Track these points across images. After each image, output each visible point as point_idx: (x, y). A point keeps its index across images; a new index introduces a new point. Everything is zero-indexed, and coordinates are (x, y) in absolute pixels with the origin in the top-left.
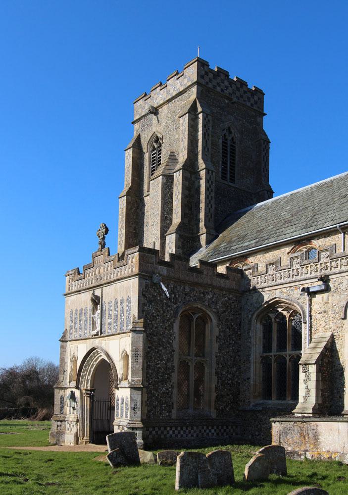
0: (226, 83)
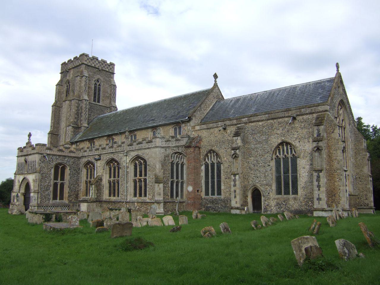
0: (97, 62)
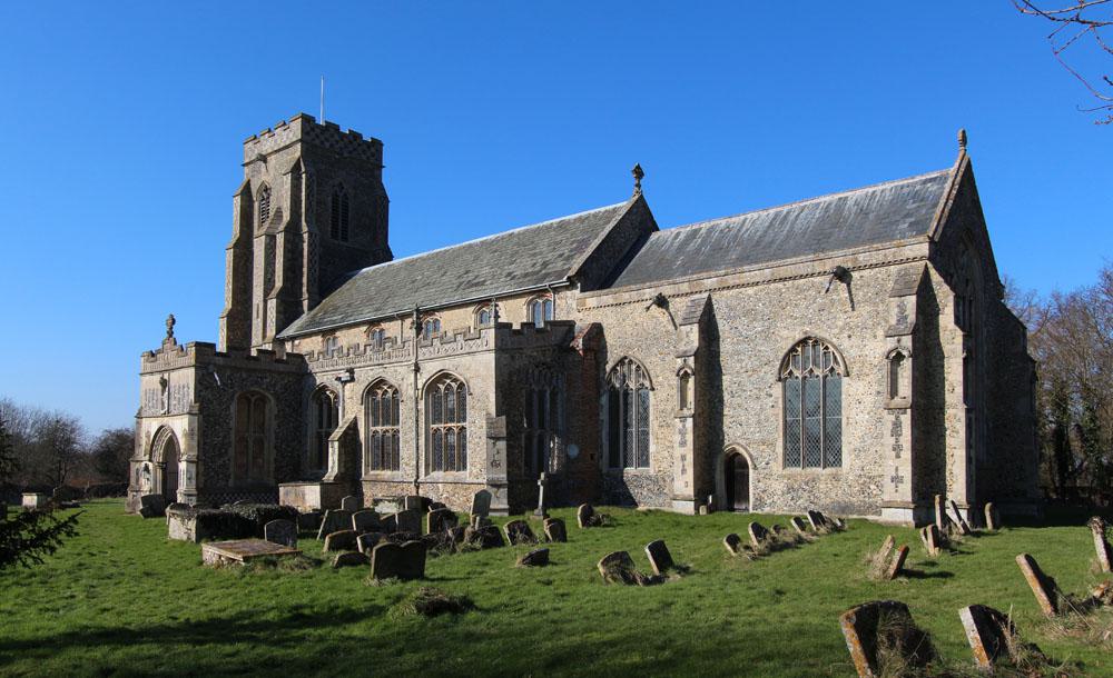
0: (337, 137)
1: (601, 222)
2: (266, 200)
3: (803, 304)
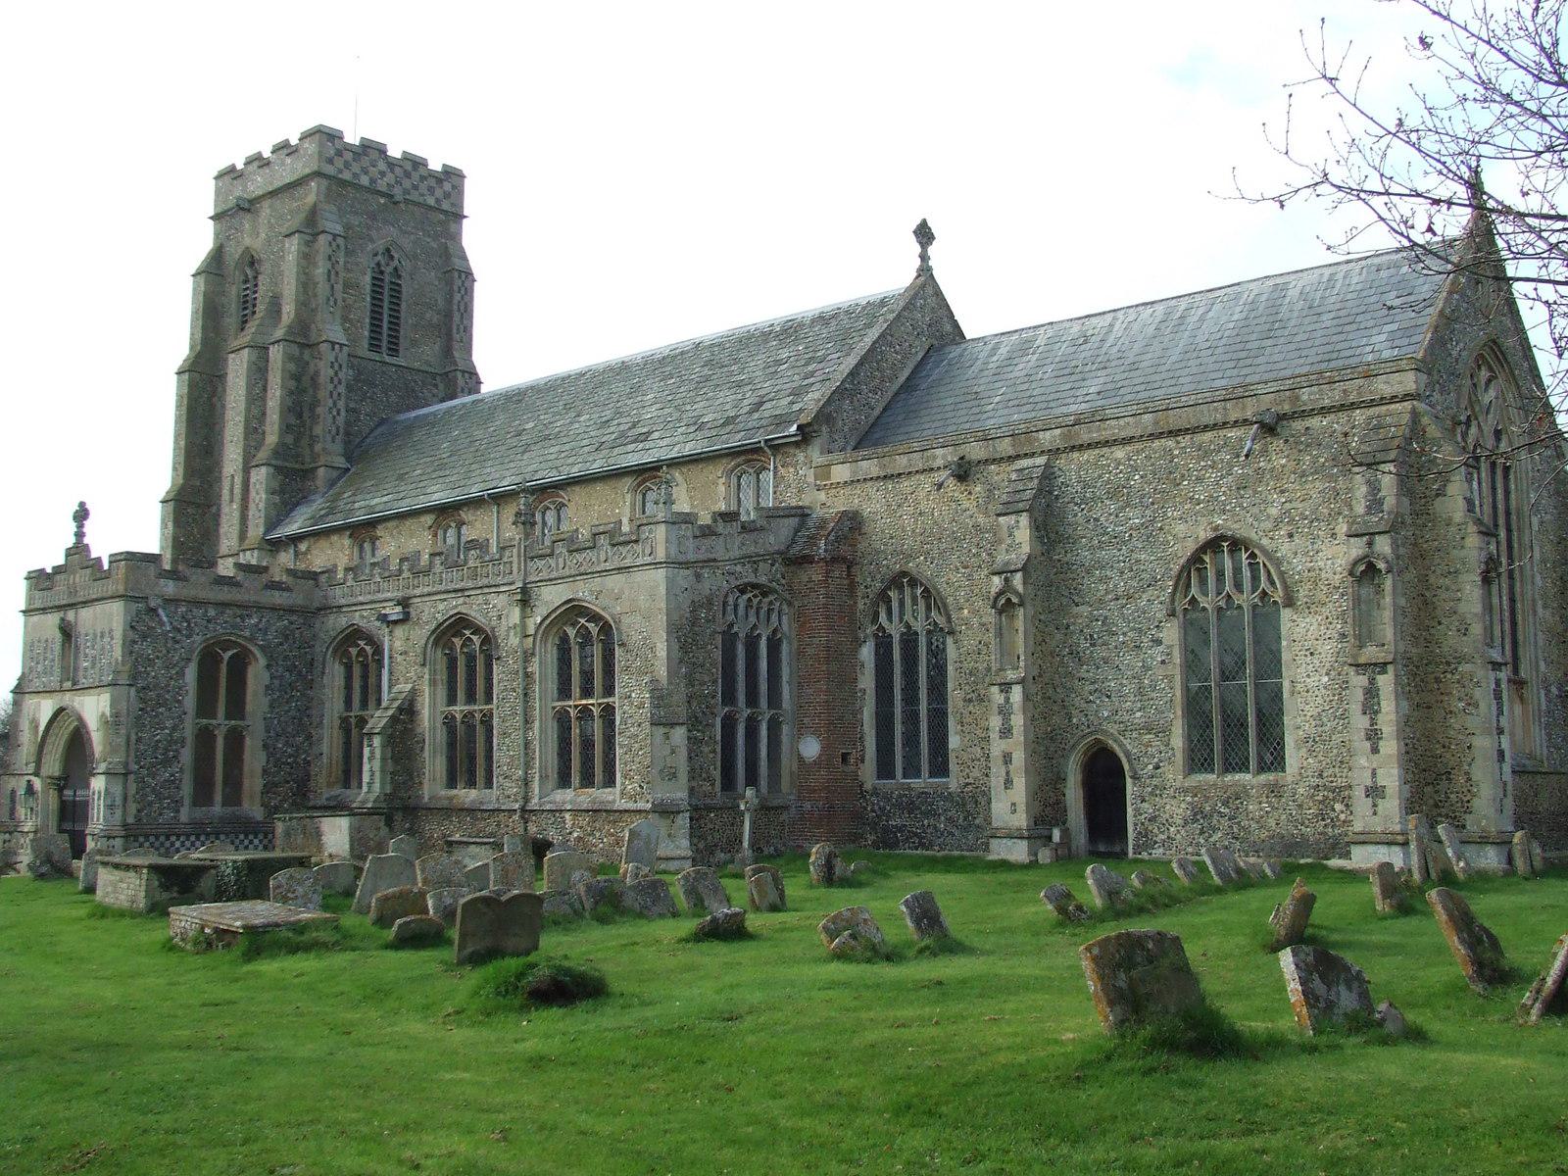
1: (860, 324)
2: (251, 282)
3: (1212, 476)
